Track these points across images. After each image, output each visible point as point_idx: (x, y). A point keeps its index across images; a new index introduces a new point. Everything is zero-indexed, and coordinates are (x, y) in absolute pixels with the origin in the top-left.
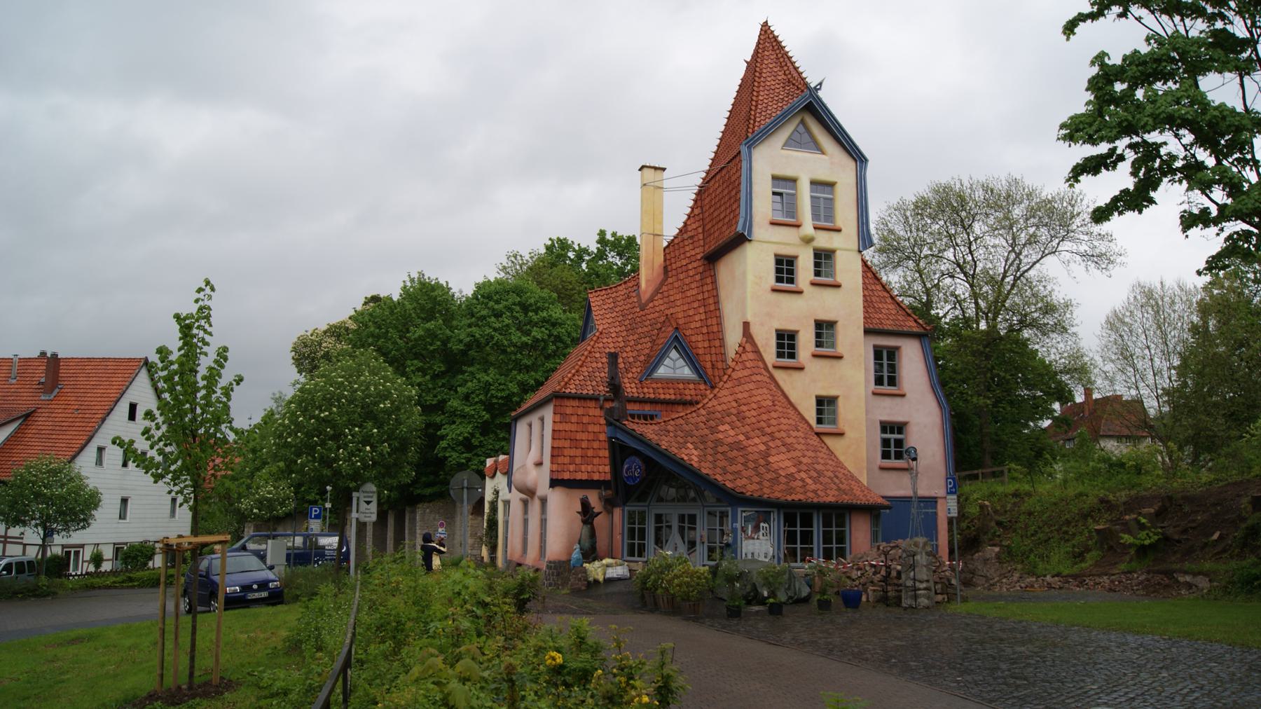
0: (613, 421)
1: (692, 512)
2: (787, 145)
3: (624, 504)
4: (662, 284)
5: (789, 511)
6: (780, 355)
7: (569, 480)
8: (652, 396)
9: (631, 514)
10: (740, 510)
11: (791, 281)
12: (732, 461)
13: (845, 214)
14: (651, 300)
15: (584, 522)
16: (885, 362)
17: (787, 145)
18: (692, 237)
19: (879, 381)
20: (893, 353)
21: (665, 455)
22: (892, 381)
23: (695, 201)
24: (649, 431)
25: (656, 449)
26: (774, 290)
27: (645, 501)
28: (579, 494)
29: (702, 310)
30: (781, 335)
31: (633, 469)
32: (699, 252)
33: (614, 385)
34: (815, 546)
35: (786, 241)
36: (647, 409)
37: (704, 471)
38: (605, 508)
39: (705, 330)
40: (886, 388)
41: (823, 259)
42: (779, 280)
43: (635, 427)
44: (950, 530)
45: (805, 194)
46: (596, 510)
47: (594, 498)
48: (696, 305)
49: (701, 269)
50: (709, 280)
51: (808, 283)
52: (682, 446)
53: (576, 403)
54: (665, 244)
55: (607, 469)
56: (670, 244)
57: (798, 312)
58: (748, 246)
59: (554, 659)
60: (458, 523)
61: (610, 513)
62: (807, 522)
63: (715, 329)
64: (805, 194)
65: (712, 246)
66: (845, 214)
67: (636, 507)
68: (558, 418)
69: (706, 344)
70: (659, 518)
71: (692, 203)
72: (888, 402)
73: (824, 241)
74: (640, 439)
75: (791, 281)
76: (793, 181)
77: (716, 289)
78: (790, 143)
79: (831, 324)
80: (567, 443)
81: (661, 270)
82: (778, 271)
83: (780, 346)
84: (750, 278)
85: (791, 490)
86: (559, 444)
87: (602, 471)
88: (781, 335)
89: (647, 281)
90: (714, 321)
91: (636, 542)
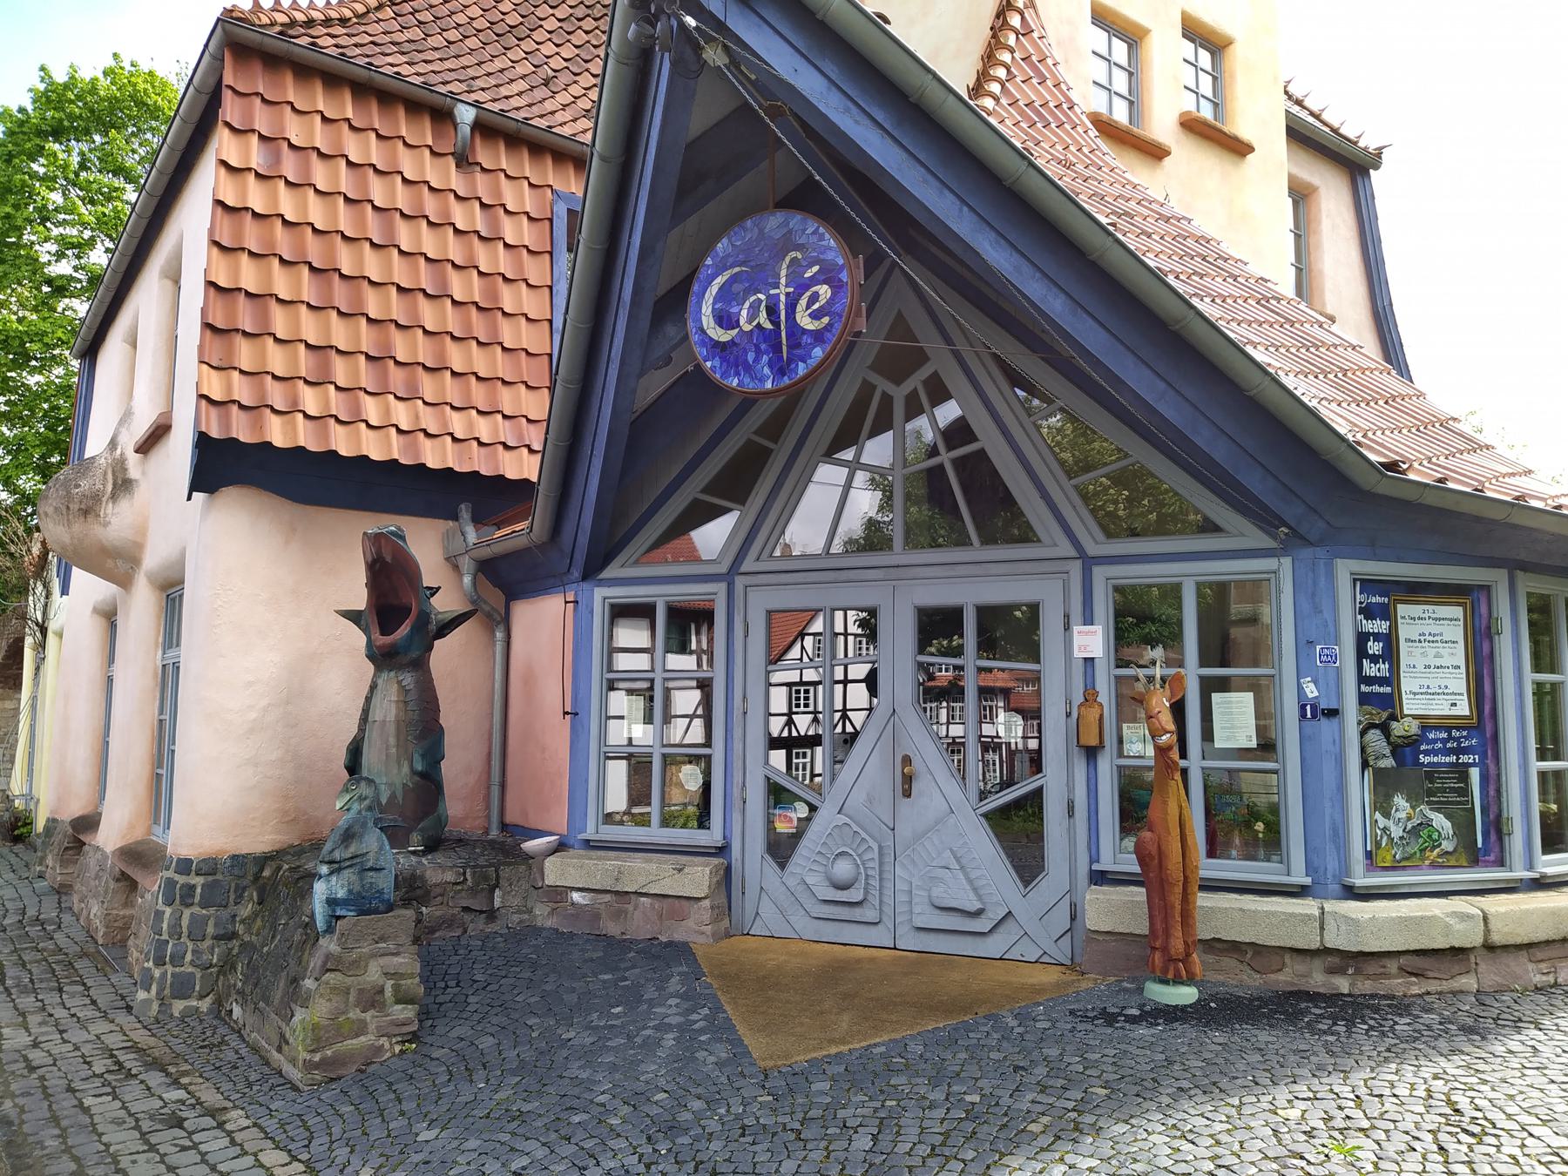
10: (1345, 569)
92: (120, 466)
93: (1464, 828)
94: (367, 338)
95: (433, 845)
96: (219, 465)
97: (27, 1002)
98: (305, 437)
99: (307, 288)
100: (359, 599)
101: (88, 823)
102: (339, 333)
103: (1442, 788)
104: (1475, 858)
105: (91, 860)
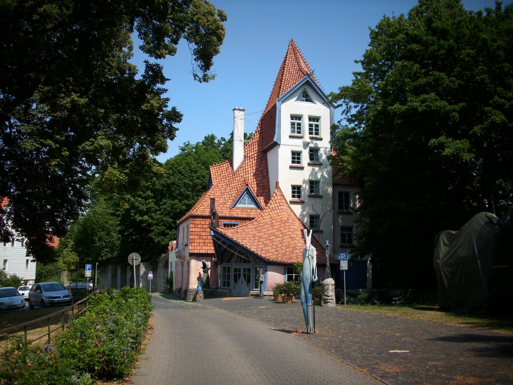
0: (213, 227)
1: (249, 267)
2: (297, 100)
4: (243, 164)
6: (293, 196)
8: (235, 216)
9: (225, 268)
11: (299, 162)
12: (266, 245)
17: (297, 100)
24: (229, 233)
25: (230, 240)
26: (291, 167)
27: (229, 263)
30: (293, 187)
33: (213, 213)
35: (297, 145)
36: (233, 222)
37: (252, 250)
42: (293, 162)
45: (306, 123)
50: (264, 161)
52: (244, 239)
55: (212, 248)
59: (74, 351)
60: (158, 271)
63: (266, 184)
64: (306, 123)
67: (227, 265)
70: (236, 270)
75: (299, 162)
76: (299, 118)
77: (268, 175)
82: (293, 158)
85: (291, 258)
87: (211, 249)
88: (293, 187)
91: (226, 280)
94: (203, 241)
102: (201, 241)
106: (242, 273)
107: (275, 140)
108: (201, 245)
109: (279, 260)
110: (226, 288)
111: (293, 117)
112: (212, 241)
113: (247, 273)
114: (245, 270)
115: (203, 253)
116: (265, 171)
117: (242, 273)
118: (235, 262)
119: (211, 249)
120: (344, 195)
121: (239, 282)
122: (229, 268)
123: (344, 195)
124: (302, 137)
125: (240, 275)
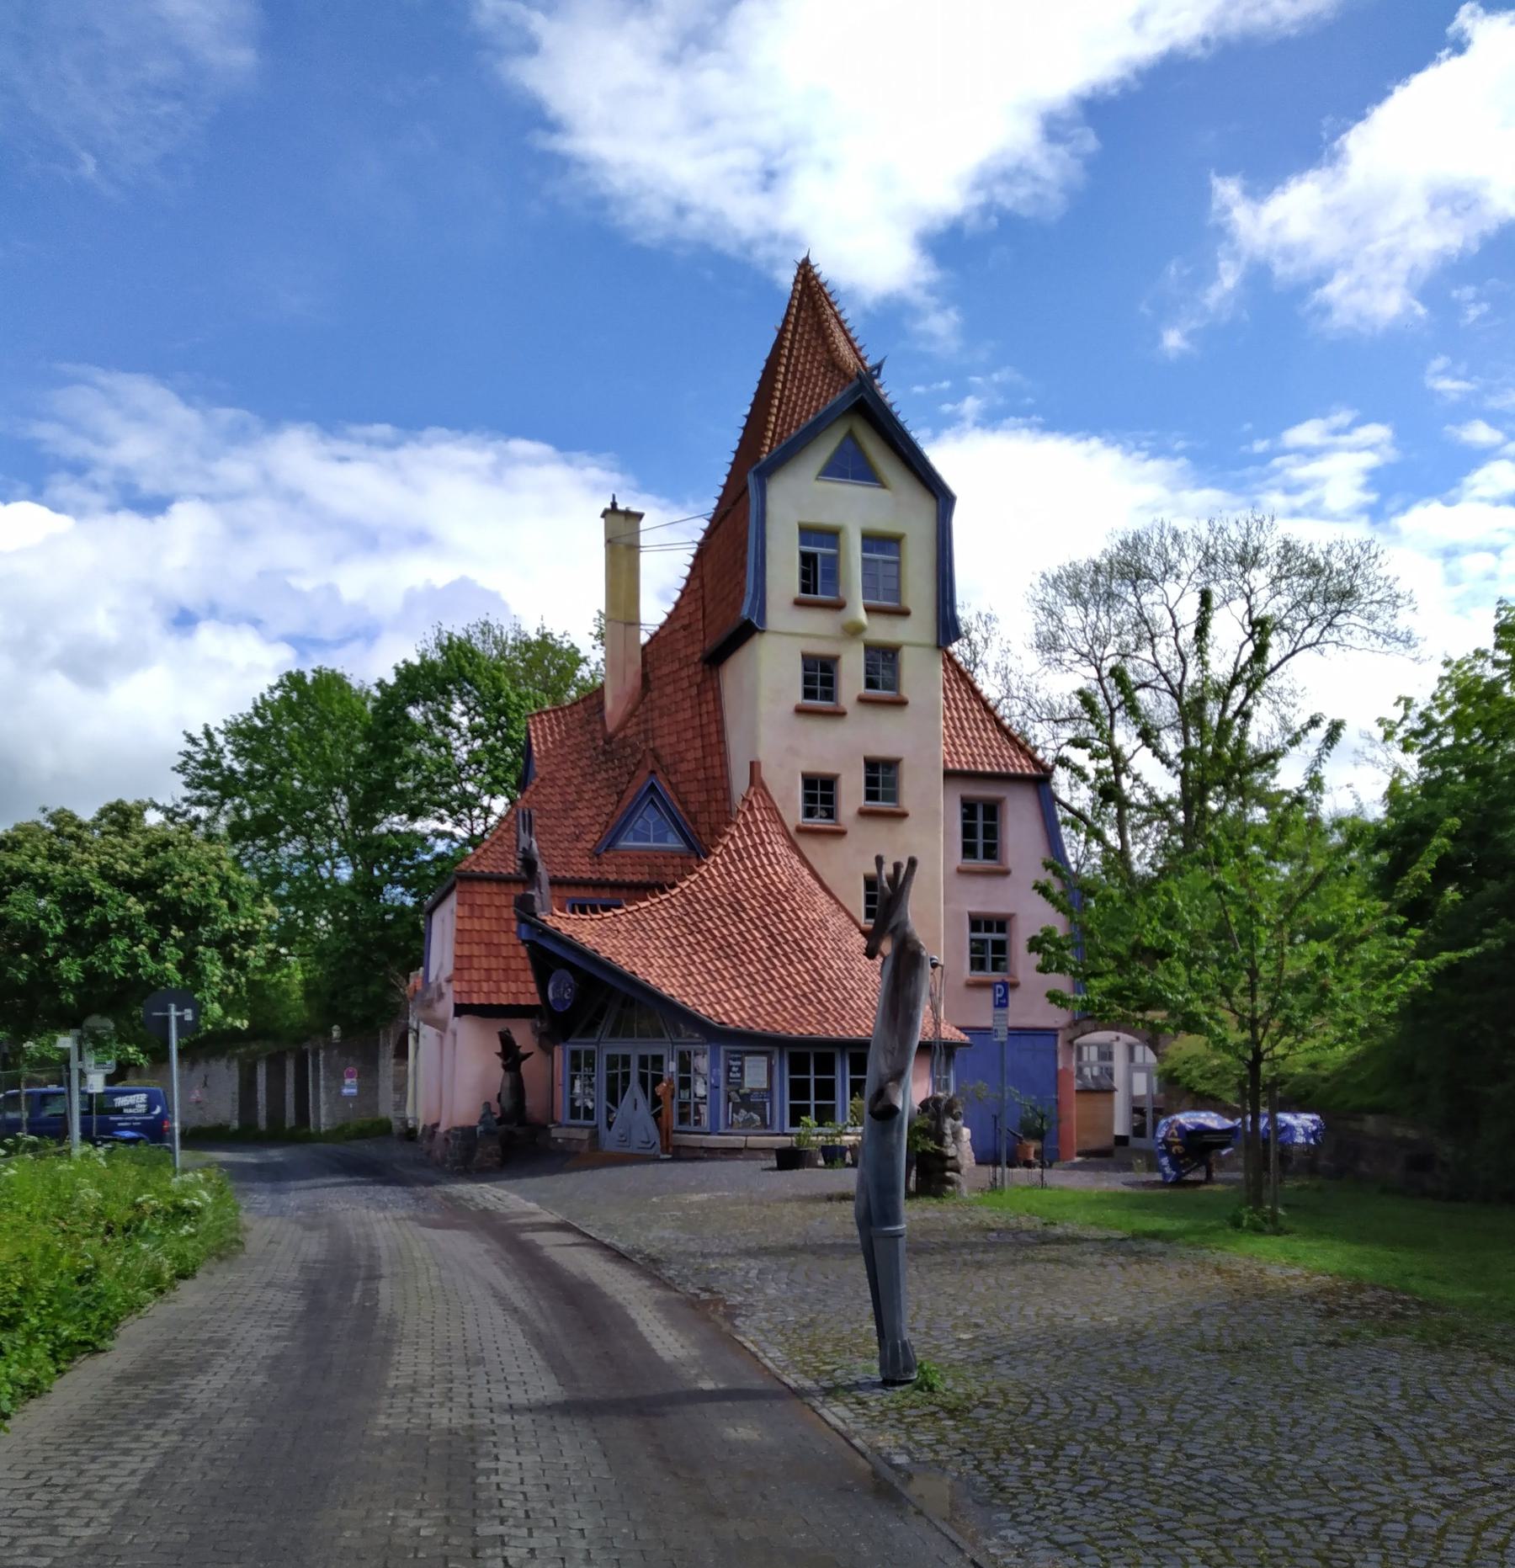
1: (657, 1051)
3: (565, 1040)
5: (854, 1051)
6: (809, 813)
7: (481, 1005)
8: (612, 878)
9: (575, 1055)
10: (722, 1048)
13: (918, 591)
14: (622, 726)
15: (506, 1067)
16: (980, 822)
18: (685, 628)
19: (969, 850)
20: (992, 810)
21: (607, 967)
22: (991, 852)
23: (693, 567)
25: (591, 958)
27: (594, 1036)
28: (501, 1024)
29: (698, 743)
30: (810, 781)
31: (561, 990)
32: (696, 651)
34: (838, 1102)
36: (606, 895)
38: (541, 1045)
39: (701, 775)
40: (980, 863)
41: (883, 662)
42: (809, 694)
43: (562, 925)
44: (69, 1078)
46: (522, 1051)
47: (523, 1034)
48: (689, 734)
49: (699, 678)
50: (710, 696)
51: (855, 697)
53: (494, 888)
54: (644, 638)
56: (654, 637)
57: (840, 748)
58: (757, 636)
61: (549, 1053)
62: (826, 1064)
63: (717, 772)
65: (710, 644)
66: (918, 591)
67: (581, 1045)
68: (466, 911)
69: (703, 797)
70: (612, 1061)
71: (687, 571)
72: (981, 884)
73: (882, 631)
74: (568, 943)
76: (831, 535)
78: (835, 470)
79: (892, 765)
80: (476, 950)
81: (638, 682)
82: (807, 680)
83: (809, 798)
84: (765, 692)
86: (466, 950)
88: (810, 781)
89: (615, 698)
90: (716, 760)
92: (439, 987)
93: (763, 1119)
94: (502, 963)
95: (519, 1125)
96: (461, 1010)
97: (435, 1283)
98: (484, 1001)
99: (482, 950)
100: (499, 1050)
101: (437, 1125)
102: (494, 963)
103: (759, 1108)
104: (766, 1127)
105: (437, 1137)
106: (634, 1071)
107: (745, 612)
108: (494, 975)
109: (760, 1025)
110: (581, 1121)
111: (808, 533)
112: (523, 951)
113: (650, 1072)
114: (643, 1061)
115: (501, 1005)
116: (713, 728)
117: (634, 1071)
118: (613, 1034)
119: (528, 995)
120: (831, 551)
121: (626, 1104)
122: (590, 1055)
123: (831, 551)
124: (839, 606)
125: (626, 1076)
